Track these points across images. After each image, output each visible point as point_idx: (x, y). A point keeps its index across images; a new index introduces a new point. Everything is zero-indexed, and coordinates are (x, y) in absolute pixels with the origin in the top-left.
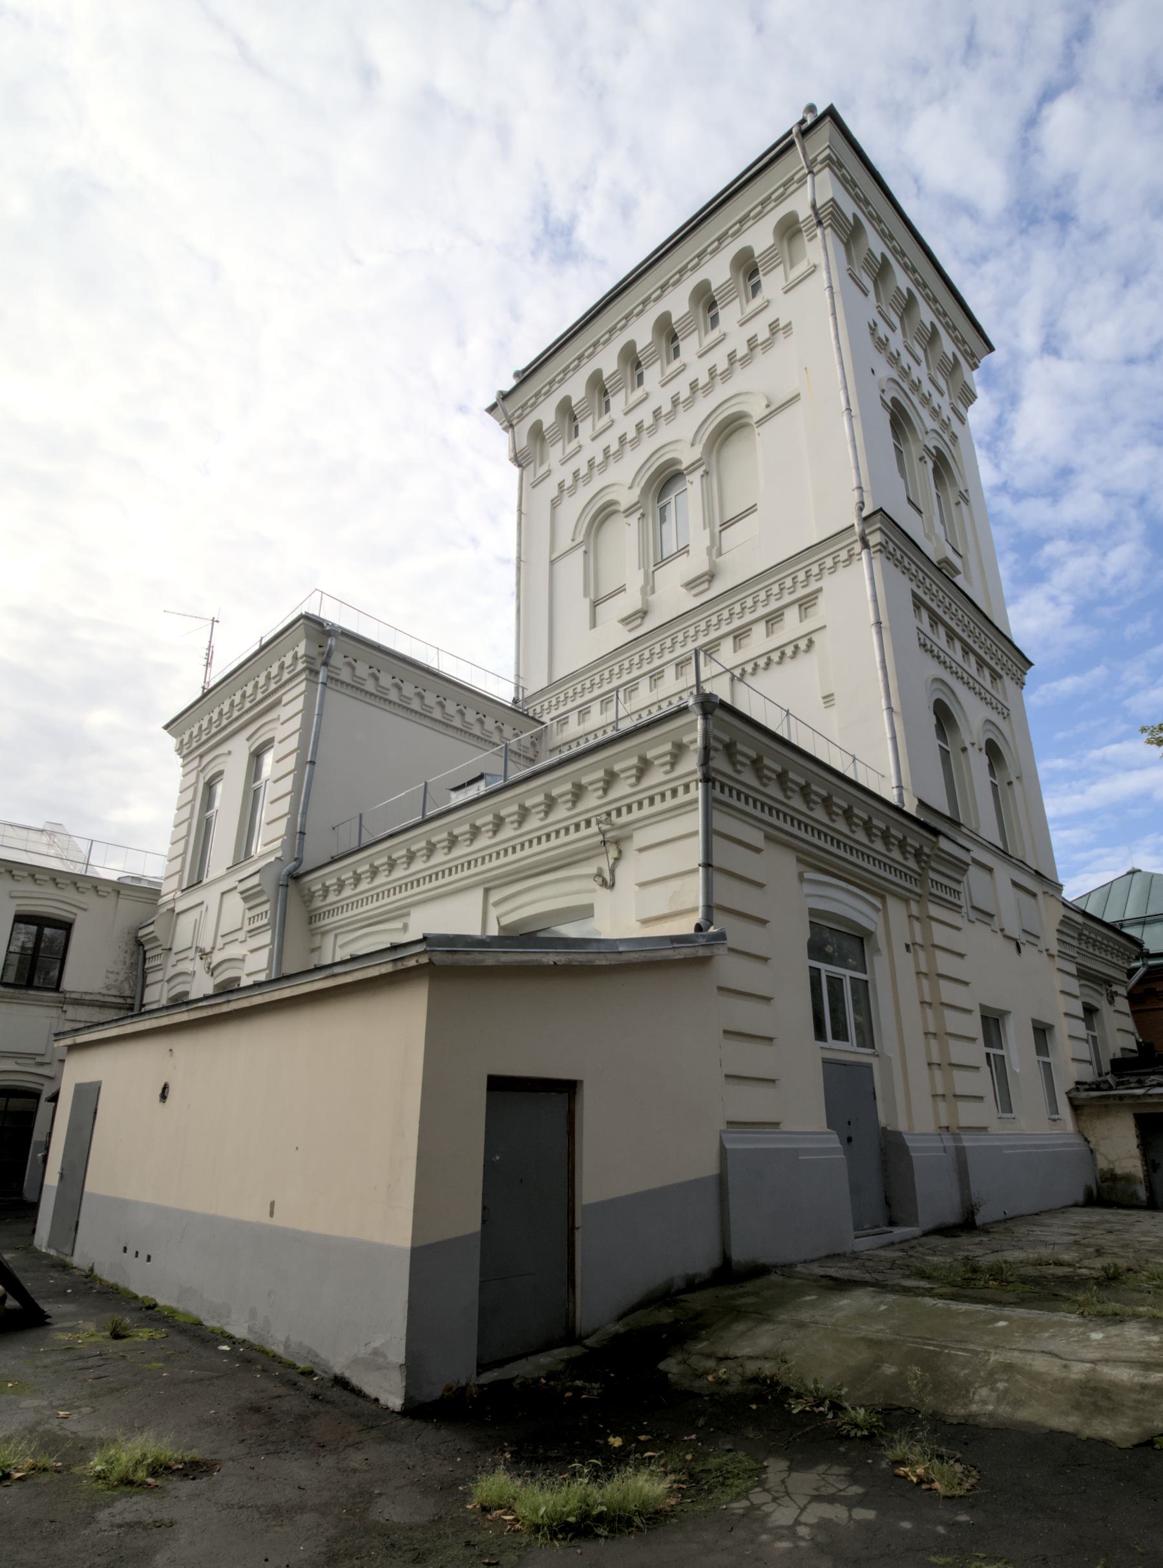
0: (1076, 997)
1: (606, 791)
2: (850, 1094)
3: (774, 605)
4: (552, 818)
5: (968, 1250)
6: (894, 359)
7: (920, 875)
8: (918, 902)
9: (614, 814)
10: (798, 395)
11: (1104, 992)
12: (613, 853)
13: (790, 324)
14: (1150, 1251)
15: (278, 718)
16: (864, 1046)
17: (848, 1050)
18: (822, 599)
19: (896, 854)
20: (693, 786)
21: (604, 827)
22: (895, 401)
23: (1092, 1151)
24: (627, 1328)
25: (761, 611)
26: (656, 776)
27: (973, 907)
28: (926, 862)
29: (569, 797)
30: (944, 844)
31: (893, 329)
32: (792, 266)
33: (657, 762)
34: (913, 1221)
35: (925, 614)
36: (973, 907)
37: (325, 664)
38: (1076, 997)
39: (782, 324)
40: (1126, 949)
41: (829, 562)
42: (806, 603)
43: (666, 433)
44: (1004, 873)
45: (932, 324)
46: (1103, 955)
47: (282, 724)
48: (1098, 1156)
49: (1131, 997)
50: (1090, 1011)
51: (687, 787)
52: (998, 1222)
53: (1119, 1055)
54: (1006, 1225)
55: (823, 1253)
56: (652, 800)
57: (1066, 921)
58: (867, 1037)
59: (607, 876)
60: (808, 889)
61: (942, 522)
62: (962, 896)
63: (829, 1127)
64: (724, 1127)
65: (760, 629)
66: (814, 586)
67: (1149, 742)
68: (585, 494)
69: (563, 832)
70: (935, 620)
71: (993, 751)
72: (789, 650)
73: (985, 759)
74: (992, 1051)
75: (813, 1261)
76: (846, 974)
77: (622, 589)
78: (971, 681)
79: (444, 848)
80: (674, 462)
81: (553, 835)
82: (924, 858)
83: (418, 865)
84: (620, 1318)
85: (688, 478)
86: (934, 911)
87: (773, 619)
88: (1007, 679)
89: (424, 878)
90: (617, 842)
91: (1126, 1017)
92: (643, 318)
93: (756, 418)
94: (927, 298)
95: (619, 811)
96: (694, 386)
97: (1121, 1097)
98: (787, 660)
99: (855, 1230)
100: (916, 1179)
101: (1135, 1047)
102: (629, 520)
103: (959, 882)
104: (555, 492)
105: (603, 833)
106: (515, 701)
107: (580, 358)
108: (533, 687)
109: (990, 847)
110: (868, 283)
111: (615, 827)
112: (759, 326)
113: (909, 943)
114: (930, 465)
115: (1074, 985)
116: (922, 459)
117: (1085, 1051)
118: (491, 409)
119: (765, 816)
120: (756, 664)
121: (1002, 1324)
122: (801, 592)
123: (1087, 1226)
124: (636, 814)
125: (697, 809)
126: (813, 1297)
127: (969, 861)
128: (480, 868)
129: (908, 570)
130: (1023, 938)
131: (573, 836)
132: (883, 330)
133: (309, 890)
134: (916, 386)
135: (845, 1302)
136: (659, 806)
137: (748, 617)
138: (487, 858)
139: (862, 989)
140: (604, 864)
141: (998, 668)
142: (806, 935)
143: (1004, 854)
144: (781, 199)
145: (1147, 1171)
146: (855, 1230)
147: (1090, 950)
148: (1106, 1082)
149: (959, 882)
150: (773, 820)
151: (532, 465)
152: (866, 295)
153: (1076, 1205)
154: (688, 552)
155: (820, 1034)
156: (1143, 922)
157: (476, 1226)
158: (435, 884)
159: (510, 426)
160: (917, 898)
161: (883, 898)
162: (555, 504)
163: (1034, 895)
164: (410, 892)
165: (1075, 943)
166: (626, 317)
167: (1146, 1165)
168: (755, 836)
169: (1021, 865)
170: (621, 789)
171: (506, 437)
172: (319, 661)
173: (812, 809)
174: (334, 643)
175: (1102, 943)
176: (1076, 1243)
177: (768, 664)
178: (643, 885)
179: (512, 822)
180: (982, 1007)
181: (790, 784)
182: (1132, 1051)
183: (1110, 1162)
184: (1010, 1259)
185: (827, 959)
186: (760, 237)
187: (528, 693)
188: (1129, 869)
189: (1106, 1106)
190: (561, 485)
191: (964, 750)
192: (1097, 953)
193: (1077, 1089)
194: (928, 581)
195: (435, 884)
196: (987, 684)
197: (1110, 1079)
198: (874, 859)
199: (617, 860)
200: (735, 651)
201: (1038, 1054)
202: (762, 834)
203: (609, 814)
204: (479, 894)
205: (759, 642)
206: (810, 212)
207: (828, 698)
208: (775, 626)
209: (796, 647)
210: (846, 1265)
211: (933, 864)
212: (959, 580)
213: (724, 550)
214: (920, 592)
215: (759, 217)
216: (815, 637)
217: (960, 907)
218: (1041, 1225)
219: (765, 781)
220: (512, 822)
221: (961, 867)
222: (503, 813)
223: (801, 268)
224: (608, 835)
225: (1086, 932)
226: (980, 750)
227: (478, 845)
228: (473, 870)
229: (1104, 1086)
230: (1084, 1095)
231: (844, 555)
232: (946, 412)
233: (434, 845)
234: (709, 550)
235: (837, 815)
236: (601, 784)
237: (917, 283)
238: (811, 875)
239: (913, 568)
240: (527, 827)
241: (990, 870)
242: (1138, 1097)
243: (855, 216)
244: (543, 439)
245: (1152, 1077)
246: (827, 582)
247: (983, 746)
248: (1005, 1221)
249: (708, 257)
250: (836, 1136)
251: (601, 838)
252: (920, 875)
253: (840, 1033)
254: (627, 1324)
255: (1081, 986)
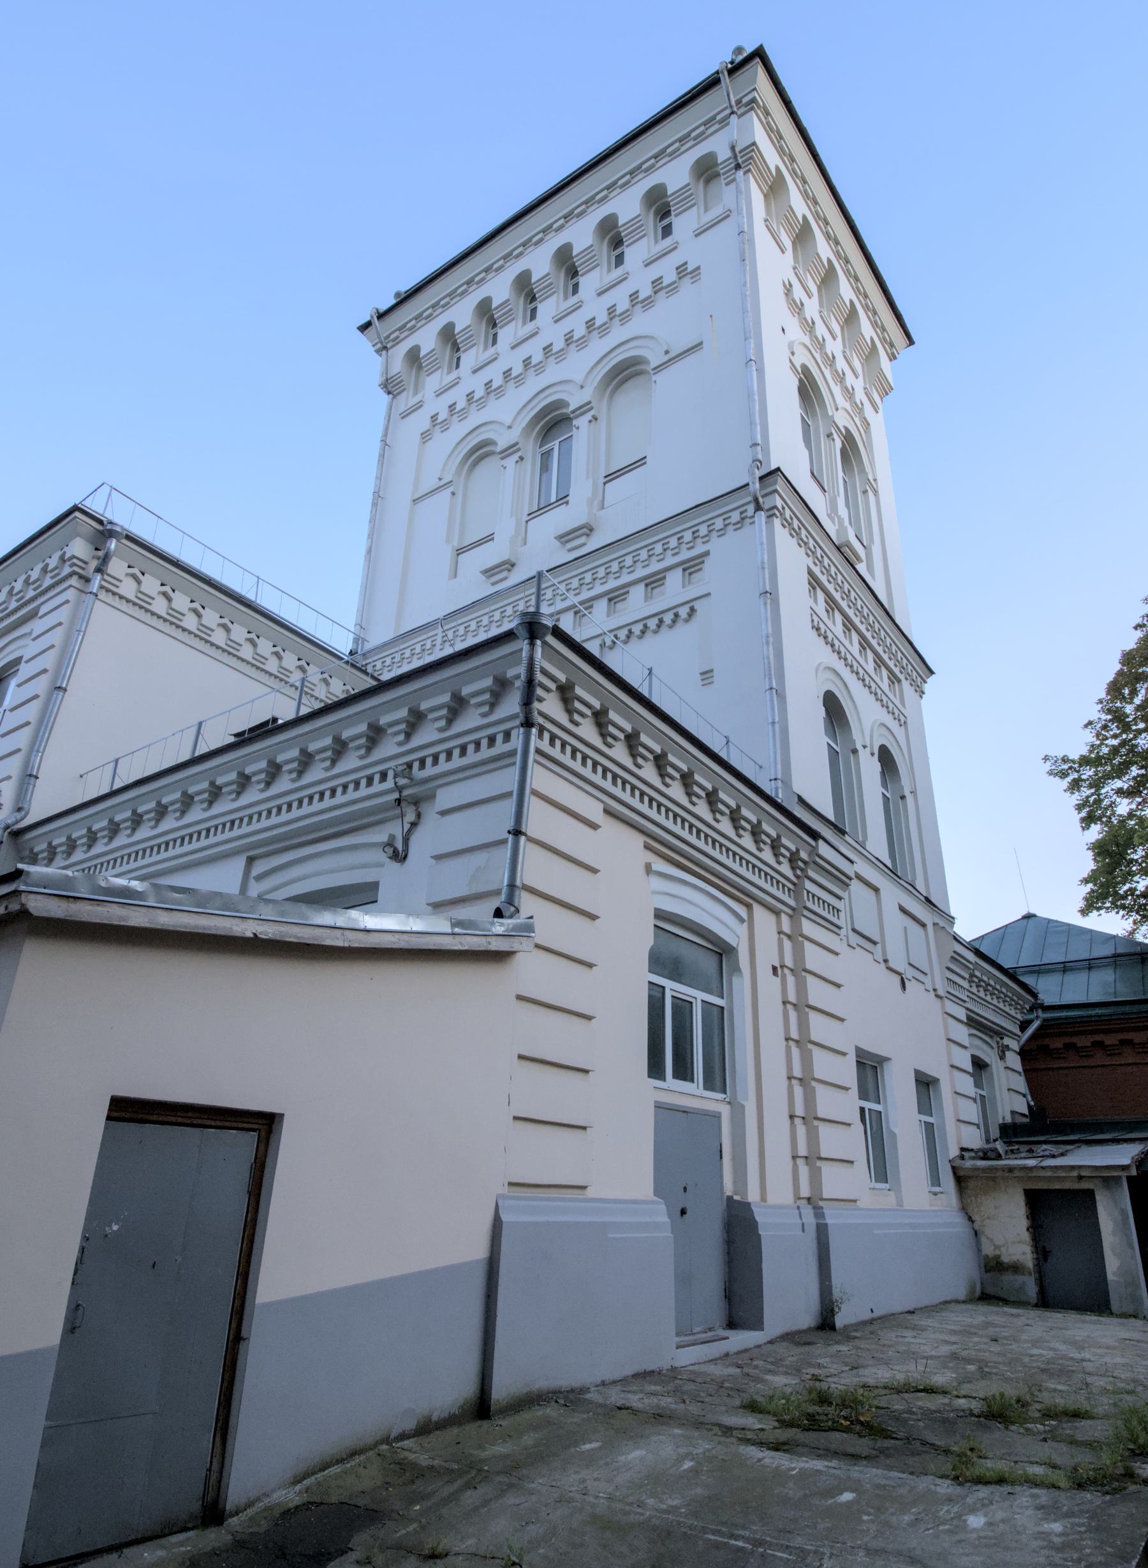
0: (965, 1047)
1: (408, 736)
2: (686, 1150)
3: (655, 567)
4: (340, 768)
5: (819, 1366)
6: (809, 327)
7: (794, 884)
8: (791, 916)
9: (416, 765)
10: (701, 343)
11: (995, 1045)
12: (410, 817)
13: (699, 268)
14: (1043, 1371)
15: (31, 633)
16: (713, 1090)
17: (691, 1094)
18: (708, 563)
19: (767, 855)
20: (514, 733)
21: (402, 781)
22: (805, 370)
23: (976, 1233)
24: (305, 1498)
25: (640, 572)
26: (470, 720)
27: (854, 930)
28: (802, 870)
29: (363, 741)
30: (823, 849)
31: (810, 296)
32: (706, 210)
33: (473, 701)
34: (757, 1324)
35: (821, 595)
36: (854, 930)
37: (99, 570)
38: (965, 1047)
39: (690, 268)
40: (1020, 997)
41: (719, 523)
42: (691, 567)
43: (554, 372)
44: (892, 895)
45: (851, 302)
46: (995, 1002)
47: (34, 639)
48: (983, 1239)
49: (1023, 1053)
50: (979, 1065)
51: (507, 735)
52: (864, 1323)
53: (1009, 1119)
54: (871, 1328)
55: (629, 1371)
56: (463, 750)
57: (956, 958)
58: (717, 1078)
59: (399, 846)
60: (656, 883)
61: (847, 506)
62: (842, 914)
63: (655, 1194)
64: (505, 1190)
65: (638, 592)
66: (699, 549)
67: (1050, 773)
68: (458, 430)
69: (351, 787)
70: (832, 604)
71: (886, 758)
72: (668, 618)
73: (878, 767)
74: (868, 1105)
75: (614, 1382)
76: (698, 996)
77: (489, 538)
78: (866, 677)
79: (202, 802)
80: (560, 404)
81: (339, 790)
82: (800, 864)
83: (168, 823)
84: (297, 1480)
85: (575, 422)
86: (808, 928)
87: (654, 582)
88: (906, 684)
89: (175, 841)
90: (416, 802)
91: (1016, 1075)
92: (542, 248)
93: (653, 364)
94: (847, 273)
95: (422, 762)
96: (590, 324)
97: (1011, 1170)
98: (664, 629)
99: (677, 1335)
100: (764, 1266)
101: (1026, 1112)
102: (506, 462)
103: (840, 898)
104: (426, 425)
105: (399, 789)
106: (351, 653)
107: (469, 282)
108: (376, 638)
109: (876, 862)
110: (787, 242)
111: (414, 783)
112: (666, 270)
113: (777, 965)
114: (838, 444)
115: (962, 1033)
116: (829, 435)
117: (971, 1111)
118: (365, 327)
119: (607, 785)
120: (630, 632)
121: (847, 1496)
122: (685, 555)
123: (967, 1332)
124: (443, 766)
125: (514, 764)
126: (595, 1445)
127: (853, 876)
128: (246, 829)
129: (805, 544)
130: (909, 973)
131: (364, 791)
132: (798, 293)
133: (32, 850)
134: (831, 361)
135: (638, 1453)
136: (472, 757)
137: (626, 578)
138: (255, 817)
139: (717, 1019)
140: (396, 829)
141: (896, 671)
142: (648, 939)
143: (893, 873)
144: (701, 138)
145: (1037, 1259)
146: (677, 1335)
147: (982, 994)
148: (995, 1150)
149: (840, 898)
150: (617, 791)
151: (404, 394)
152: (783, 252)
153: (957, 1302)
154: (567, 503)
155: (655, 1069)
156: (1039, 970)
157: (50, 1333)
158: (187, 848)
159: (383, 349)
160: (789, 911)
161: (749, 907)
162: (426, 436)
163: (924, 925)
164: (155, 858)
165: (965, 984)
166: (524, 245)
167: (1037, 1252)
168: (592, 809)
169: (911, 887)
170: (427, 734)
171: (377, 361)
172: (94, 564)
173: (667, 785)
174: (113, 546)
175: (994, 988)
176: (954, 1356)
177: (643, 632)
178: (438, 858)
179: (290, 772)
180: (858, 1049)
181: (641, 749)
182: (1023, 1115)
183: (997, 1247)
184: (871, 1381)
185: (676, 976)
186: (675, 175)
187: (368, 646)
188: (1024, 913)
189: (994, 1179)
190: (434, 418)
191: (855, 751)
192: (988, 998)
193: (962, 1157)
194: (826, 561)
195: (187, 848)
196: (885, 685)
197: (1000, 1146)
198: (741, 858)
199: (414, 825)
200: (608, 615)
201: (920, 1112)
202: (601, 806)
203: (410, 765)
204: (240, 863)
205: (637, 605)
206: (729, 154)
207: (707, 675)
208: (655, 591)
209: (676, 615)
210: (658, 1388)
211: (811, 873)
212: (861, 568)
213: (606, 505)
214: (817, 570)
215: (675, 155)
216: (697, 605)
217: (839, 928)
218: (914, 1328)
219: (609, 740)
220: (290, 772)
221: (843, 880)
222: (280, 759)
223: (716, 212)
224: (405, 793)
225: (977, 973)
226: (872, 754)
227: (245, 800)
228: (236, 832)
229: (990, 1154)
230: (969, 1164)
231: (735, 516)
232: (860, 396)
233: (191, 798)
234: (590, 502)
235: (699, 797)
236: (403, 726)
237: (838, 255)
238: (660, 865)
239: (811, 543)
240: (308, 778)
241: (876, 890)
242: (1031, 1169)
243: (777, 168)
244: (420, 367)
245: (1045, 1147)
246: (715, 545)
247: (876, 751)
248: (871, 1322)
249: (618, 190)
250: (663, 1207)
251: (396, 795)
252: (794, 884)
253: (683, 1071)
254: (307, 1490)
255: (970, 1035)
